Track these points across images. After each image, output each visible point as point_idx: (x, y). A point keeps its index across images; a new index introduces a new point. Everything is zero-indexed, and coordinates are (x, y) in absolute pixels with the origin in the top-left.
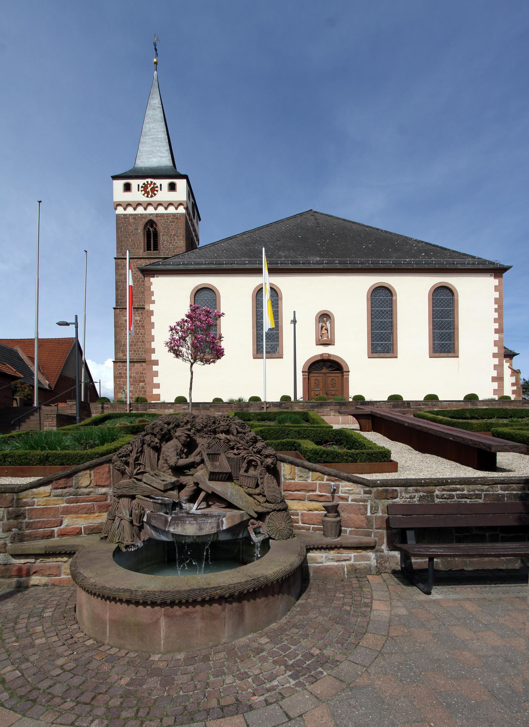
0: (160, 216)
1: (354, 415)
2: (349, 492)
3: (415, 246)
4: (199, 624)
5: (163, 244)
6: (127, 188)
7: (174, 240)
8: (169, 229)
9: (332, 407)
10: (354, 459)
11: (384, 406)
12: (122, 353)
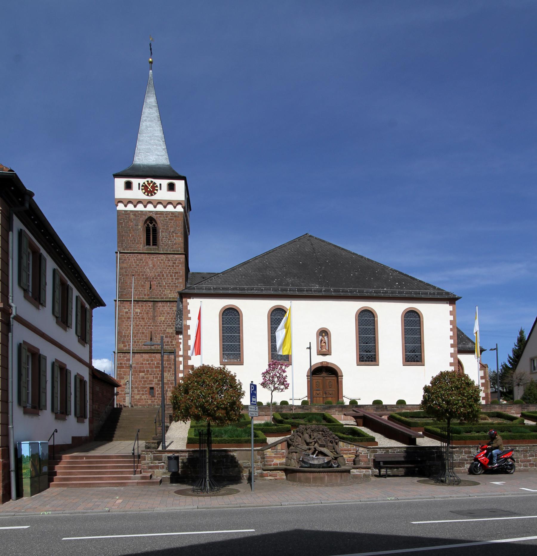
0: (159, 214)
1: (353, 417)
2: (362, 451)
3: (391, 275)
4: (334, 477)
5: (162, 240)
6: (128, 186)
7: (173, 237)
8: (168, 226)
9: (337, 409)
10: (362, 441)
11: (370, 408)
12: (123, 343)
